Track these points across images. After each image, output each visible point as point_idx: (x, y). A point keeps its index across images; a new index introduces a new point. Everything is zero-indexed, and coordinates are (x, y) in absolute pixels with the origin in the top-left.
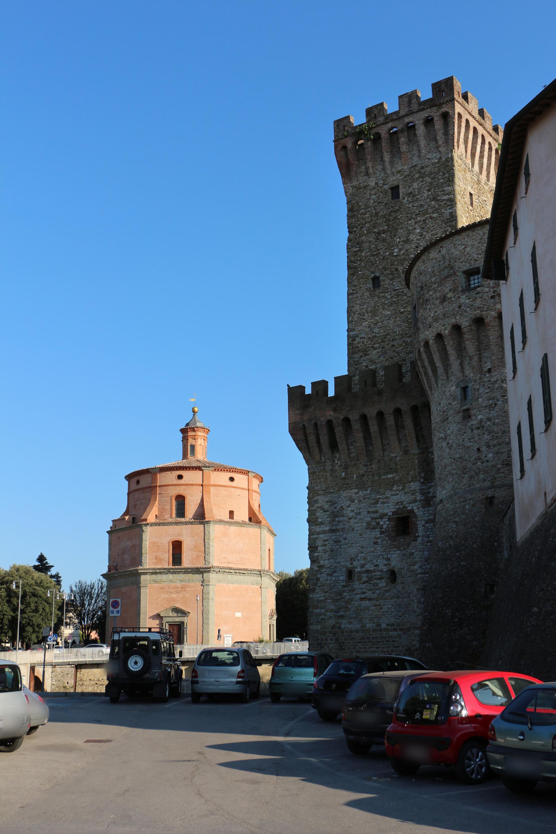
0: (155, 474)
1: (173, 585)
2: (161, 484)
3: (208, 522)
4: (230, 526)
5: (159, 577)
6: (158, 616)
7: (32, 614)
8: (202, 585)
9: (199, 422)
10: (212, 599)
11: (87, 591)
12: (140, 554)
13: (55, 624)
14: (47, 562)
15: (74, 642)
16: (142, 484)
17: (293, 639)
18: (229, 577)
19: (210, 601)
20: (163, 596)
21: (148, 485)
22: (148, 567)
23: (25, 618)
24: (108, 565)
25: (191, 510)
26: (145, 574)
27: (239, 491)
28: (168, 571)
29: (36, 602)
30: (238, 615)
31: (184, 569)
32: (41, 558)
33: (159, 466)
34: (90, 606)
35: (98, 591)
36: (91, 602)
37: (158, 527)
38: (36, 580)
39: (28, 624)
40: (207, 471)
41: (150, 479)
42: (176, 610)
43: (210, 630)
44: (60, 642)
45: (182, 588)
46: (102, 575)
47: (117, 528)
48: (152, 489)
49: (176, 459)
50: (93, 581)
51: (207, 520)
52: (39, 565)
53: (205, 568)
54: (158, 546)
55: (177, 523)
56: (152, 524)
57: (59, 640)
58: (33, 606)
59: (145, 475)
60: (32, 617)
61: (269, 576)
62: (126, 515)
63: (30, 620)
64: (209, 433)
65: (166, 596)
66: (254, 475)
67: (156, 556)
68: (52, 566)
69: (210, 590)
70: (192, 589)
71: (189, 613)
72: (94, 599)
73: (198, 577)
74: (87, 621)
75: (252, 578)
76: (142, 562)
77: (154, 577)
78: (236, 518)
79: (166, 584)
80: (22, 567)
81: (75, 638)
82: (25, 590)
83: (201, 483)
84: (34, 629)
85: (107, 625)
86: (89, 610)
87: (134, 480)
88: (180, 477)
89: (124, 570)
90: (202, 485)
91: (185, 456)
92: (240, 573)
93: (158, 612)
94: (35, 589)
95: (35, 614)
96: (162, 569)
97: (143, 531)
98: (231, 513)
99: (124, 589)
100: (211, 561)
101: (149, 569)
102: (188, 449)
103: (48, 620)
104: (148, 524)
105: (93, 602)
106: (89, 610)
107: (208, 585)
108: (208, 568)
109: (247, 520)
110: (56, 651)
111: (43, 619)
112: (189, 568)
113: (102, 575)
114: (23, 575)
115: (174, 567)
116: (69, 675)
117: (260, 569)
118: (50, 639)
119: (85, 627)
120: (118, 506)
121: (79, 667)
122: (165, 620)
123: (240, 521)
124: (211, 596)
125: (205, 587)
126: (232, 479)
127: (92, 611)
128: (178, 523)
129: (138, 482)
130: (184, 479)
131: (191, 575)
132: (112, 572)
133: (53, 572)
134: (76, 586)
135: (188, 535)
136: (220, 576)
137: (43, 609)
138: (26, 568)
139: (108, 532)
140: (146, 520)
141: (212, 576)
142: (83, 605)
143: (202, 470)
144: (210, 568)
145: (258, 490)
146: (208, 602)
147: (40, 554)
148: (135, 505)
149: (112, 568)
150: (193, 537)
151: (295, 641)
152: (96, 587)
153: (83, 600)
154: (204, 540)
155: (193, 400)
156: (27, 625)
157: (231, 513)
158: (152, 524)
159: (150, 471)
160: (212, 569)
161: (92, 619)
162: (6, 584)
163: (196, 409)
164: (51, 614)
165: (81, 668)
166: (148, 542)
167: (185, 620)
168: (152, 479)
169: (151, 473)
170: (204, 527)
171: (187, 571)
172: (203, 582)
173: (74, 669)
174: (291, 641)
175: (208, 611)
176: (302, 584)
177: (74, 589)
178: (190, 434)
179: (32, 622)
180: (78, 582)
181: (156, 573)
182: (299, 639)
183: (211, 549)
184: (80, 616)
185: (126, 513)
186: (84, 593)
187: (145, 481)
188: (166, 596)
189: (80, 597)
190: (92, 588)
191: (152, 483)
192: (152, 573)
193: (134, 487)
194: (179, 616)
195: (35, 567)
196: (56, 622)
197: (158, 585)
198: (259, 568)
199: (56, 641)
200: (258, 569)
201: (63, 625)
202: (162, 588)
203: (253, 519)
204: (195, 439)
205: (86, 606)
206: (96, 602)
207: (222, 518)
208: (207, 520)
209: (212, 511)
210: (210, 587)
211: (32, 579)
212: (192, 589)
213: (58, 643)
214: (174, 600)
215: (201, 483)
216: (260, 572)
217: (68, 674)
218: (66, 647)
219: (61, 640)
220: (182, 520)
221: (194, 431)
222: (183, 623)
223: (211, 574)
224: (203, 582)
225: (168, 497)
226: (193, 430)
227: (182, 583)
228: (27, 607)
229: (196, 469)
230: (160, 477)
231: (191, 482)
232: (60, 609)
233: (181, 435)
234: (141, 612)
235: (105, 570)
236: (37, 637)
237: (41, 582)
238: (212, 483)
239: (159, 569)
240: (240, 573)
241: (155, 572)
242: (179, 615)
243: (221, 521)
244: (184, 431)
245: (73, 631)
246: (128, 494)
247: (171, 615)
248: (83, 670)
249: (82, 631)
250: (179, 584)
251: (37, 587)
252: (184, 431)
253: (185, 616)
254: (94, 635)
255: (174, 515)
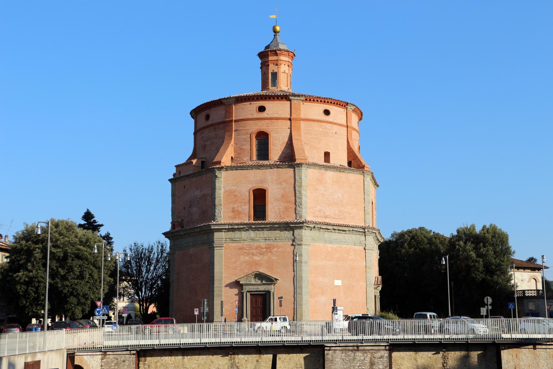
0: (230, 106)
1: (256, 244)
2: (238, 118)
3: (300, 165)
4: (326, 170)
5: (237, 234)
6: (237, 284)
7: (76, 281)
8: (292, 245)
9: (282, 44)
10: (306, 263)
11: (145, 255)
12: (213, 206)
13: (106, 295)
14: (95, 221)
15: (129, 317)
16: (212, 120)
17: (428, 314)
18: (327, 235)
19: (303, 264)
20: (242, 258)
21: (221, 120)
22: (223, 222)
23: (67, 286)
24: (171, 221)
25: (276, 150)
26: (220, 230)
27: (336, 128)
28: (248, 227)
29: (80, 266)
30: (338, 283)
31: (270, 224)
32: (88, 216)
33: (235, 96)
34: (148, 274)
35: (158, 255)
36: (150, 269)
37: (234, 172)
38: (80, 238)
39: (72, 294)
40: (296, 101)
41: (223, 112)
42: (260, 276)
43: (304, 302)
44: (113, 316)
45: (267, 248)
46: (164, 234)
47: (181, 175)
48: (226, 125)
49: (257, 90)
50: (152, 244)
51: (298, 162)
52: (85, 224)
53: (297, 223)
54: (236, 196)
55: (259, 167)
56: (227, 168)
57: (111, 313)
58: (77, 270)
59: (217, 108)
60: (76, 285)
61: (374, 235)
62: (194, 159)
63: (74, 289)
64: (295, 58)
65: (247, 258)
66: (353, 108)
67: (233, 208)
68: (102, 225)
69: (303, 250)
70: (280, 250)
71: (276, 279)
72: (153, 265)
73: (288, 234)
74: (145, 292)
75: (354, 236)
76: (215, 215)
77: (231, 234)
78: (333, 161)
79: (246, 243)
80: (62, 222)
81: (131, 312)
82: (67, 250)
83: (289, 116)
84: (79, 300)
85: (171, 296)
86: (147, 278)
87: (202, 115)
88: (262, 109)
89: (192, 227)
90: (290, 119)
91: (265, 86)
92: (339, 230)
93: (236, 278)
94: (79, 250)
95: (80, 281)
96: (241, 224)
97: (216, 176)
98: (327, 155)
99: (191, 251)
100: (304, 214)
101: (225, 224)
102: (268, 77)
103: (97, 289)
104: (222, 168)
105: (152, 268)
106: (147, 278)
107: (301, 245)
108: (300, 223)
109: (346, 165)
110: (108, 328)
111: (90, 288)
112: (276, 224)
113: (164, 234)
114: (64, 231)
115: (257, 222)
116: (127, 363)
117: (363, 225)
118: (99, 312)
119: (143, 298)
120: (182, 148)
121: (142, 353)
122: (246, 289)
123: (338, 165)
124: (304, 259)
125: (296, 247)
126: (327, 112)
127: (151, 280)
128: (261, 166)
129: (208, 117)
130: (266, 111)
131: (278, 231)
132: (177, 229)
133: (103, 232)
134: (131, 249)
135: (274, 181)
136: (315, 233)
137: (90, 275)
138: (67, 223)
139: (170, 180)
140: (219, 163)
141: (305, 234)
142: (139, 272)
143: (290, 100)
144: (303, 223)
145: (357, 128)
146: (301, 266)
147: (86, 211)
148: (205, 146)
149: (176, 224)
150: (280, 183)
151: (430, 316)
152: (155, 250)
153: (140, 266)
154: (295, 187)
155: (274, 17)
156: (70, 296)
157: (327, 155)
158: (227, 168)
159: (224, 101)
160: (305, 225)
161: (151, 290)
162: (42, 243)
163: (278, 28)
164: (100, 282)
165: (145, 356)
166: (223, 190)
167: (271, 288)
168: (226, 112)
169: (224, 104)
170: (294, 171)
171: (273, 227)
172: (293, 241)
173: (133, 358)
174: (425, 317)
175: (301, 277)
176: (404, 248)
177: (129, 252)
178: (271, 58)
179: (77, 290)
180: (133, 245)
181: (233, 230)
182: (435, 314)
183: (304, 199)
184: (137, 287)
185: (193, 156)
186: (141, 257)
187: (217, 115)
188: (247, 258)
189: (136, 262)
190: (151, 252)
191: (226, 117)
192: (229, 230)
193: (203, 123)
194: (264, 284)
195: (80, 226)
196: (106, 291)
197: (235, 244)
198: (362, 224)
199: (108, 315)
200: (361, 225)
201: (116, 296)
202: (241, 249)
203: (354, 163)
204: (277, 65)
205: (144, 274)
206: (155, 269)
207: (315, 161)
208: (298, 162)
209: (304, 151)
210: (303, 247)
211: (76, 237)
212: (280, 250)
213: (109, 318)
214: (256, 264)
215: (289, 116)
216: (364, 229)
217: (124, 361)
218: (121, 323)
219: (114, 314)
220: (266, 162)
221: (276, 54)
222: (269, 292)
223: (303, 231)
224: (293, 241)
225: (247, 134)
226: (275, 53)
227: (267, 242)
228: (69, 272)
229: (282, 98)
230: (236, 109)
231: (276, 116)
232: (113, 274)
233: (259, 61)
234: (215, 278)
235: (168, 227)
236: (83, 311)
237: (87, 240)
238: (302, 116)
239: (238, 224)
240: (339, 230)
241: (232, 228)
242: (264, 282)
243: (315, 165)
244: (263, 55)
245: (127, 303)
246: (195, 134)
247: (253, 282)
248: (148, 359)
249: (139, 303)
250: (263, 244)
251: (81, 247)
252: (263, 55)
253: (271, 284)
254: (152, 309)
255: (255, 158)
